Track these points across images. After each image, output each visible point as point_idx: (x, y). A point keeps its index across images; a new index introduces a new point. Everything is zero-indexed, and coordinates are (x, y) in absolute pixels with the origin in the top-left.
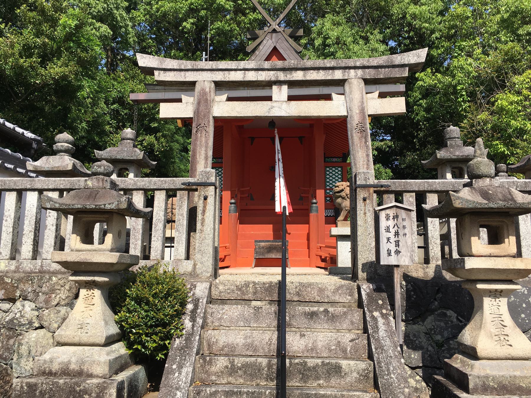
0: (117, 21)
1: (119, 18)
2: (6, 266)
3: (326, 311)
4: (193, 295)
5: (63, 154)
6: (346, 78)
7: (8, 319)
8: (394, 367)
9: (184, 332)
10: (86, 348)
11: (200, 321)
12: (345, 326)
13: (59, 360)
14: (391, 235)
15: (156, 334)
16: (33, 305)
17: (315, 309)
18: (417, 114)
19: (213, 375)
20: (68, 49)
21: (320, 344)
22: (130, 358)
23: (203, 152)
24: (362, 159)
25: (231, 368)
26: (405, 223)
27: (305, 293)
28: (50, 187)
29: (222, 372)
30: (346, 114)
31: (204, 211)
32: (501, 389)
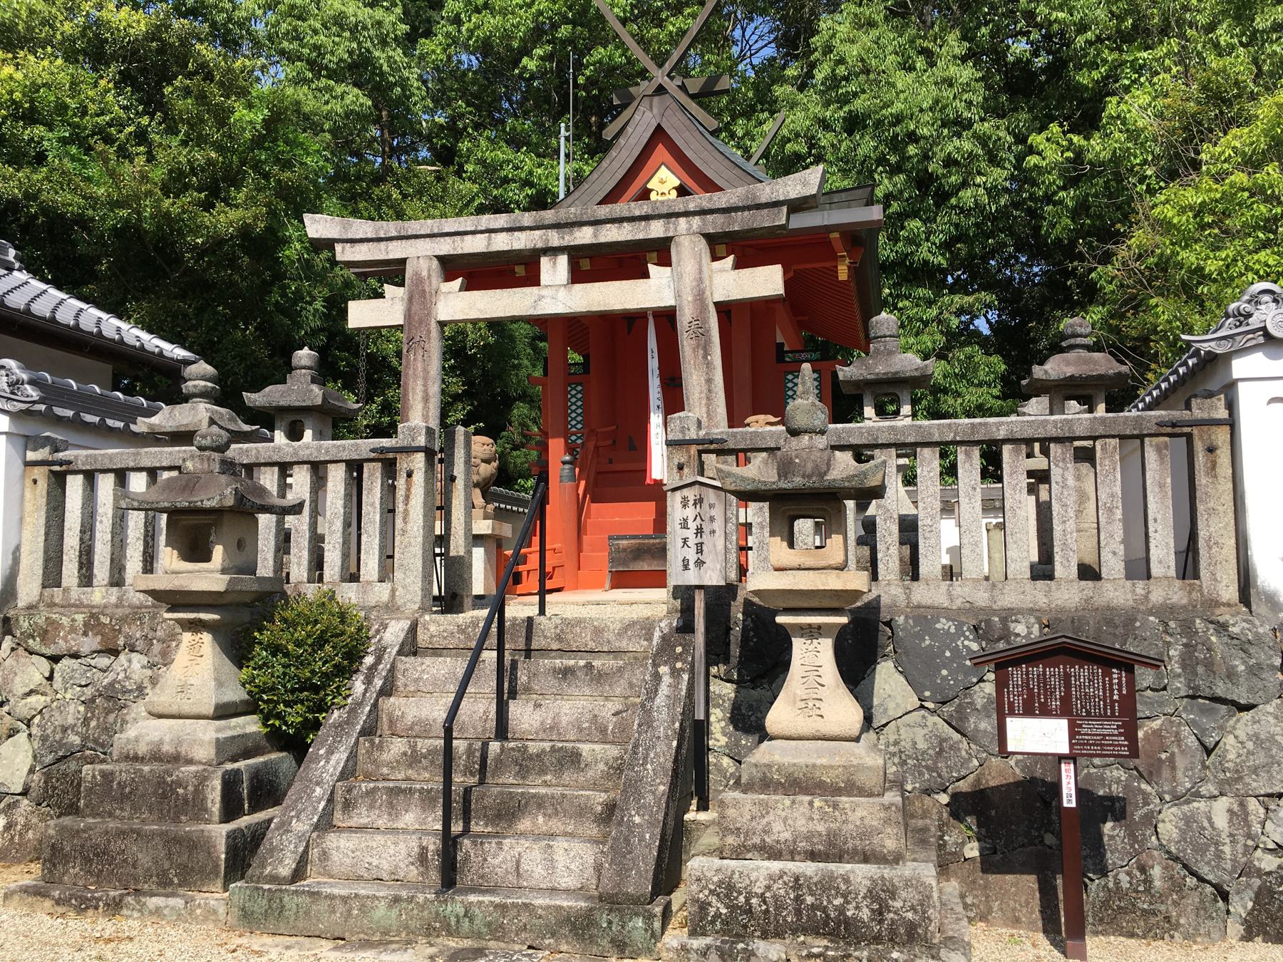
0: (382, 74)
1: (385, 68)
2: (104, 597)
3: (589, 666)
6: (671, 234)
7: (106, 682)
8: (656, 754)
9: (349, 700)
10: (188, 721)
11: (378, 683)
12: (618, 691)
13: (148, 739)
14: (690, 534)
15: (302, 702)
16: (144, 660)
17: (572, 662)
18: (1053, 226)
20: (257, 166)
21: (564, 720)
22: (268, 741)
23: (419, 389)
24: (698, 388)
25: (412, 756)
26: (713, 512)
27: (570, 636)
28: (164, 464)
29: (398, 762)
30: (671, 302)
31: (407, 497)
32: (790, 786)
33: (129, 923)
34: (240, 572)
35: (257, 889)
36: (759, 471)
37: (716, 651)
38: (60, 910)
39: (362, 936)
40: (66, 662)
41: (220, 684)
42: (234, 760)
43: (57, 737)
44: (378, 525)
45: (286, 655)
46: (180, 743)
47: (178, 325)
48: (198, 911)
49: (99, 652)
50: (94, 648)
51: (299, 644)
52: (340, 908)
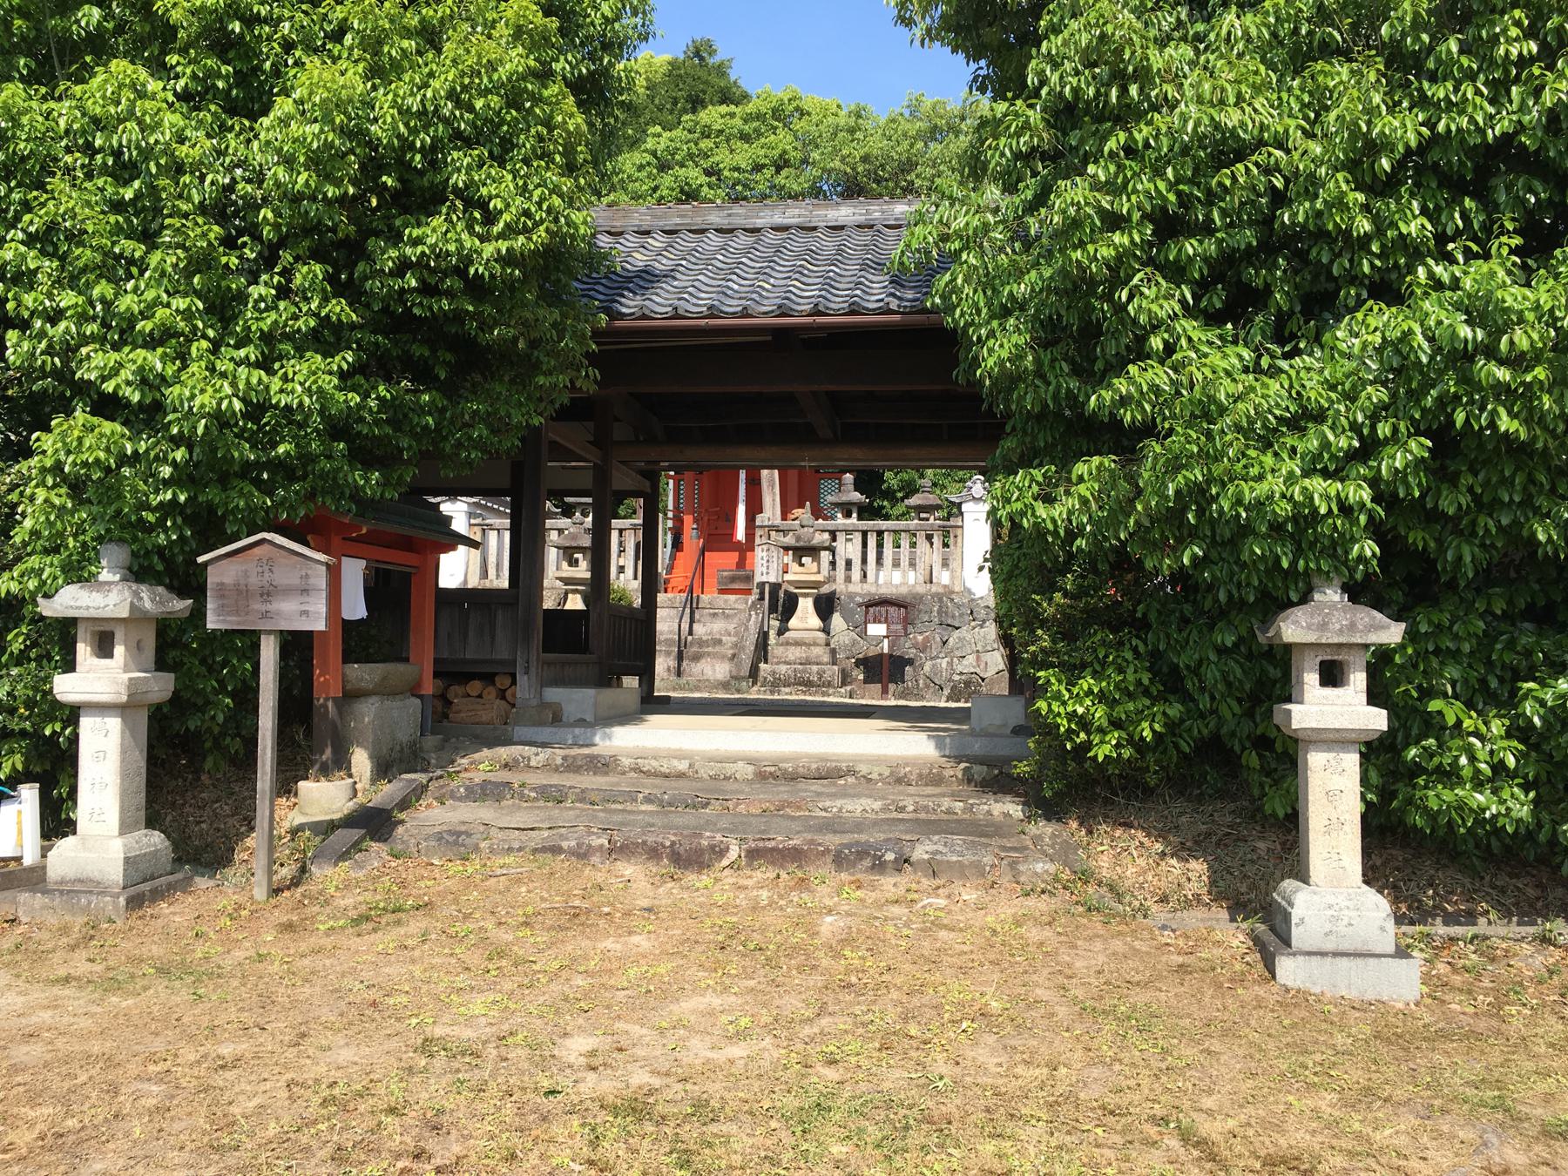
36: (789, 540)
37: (773, 608)
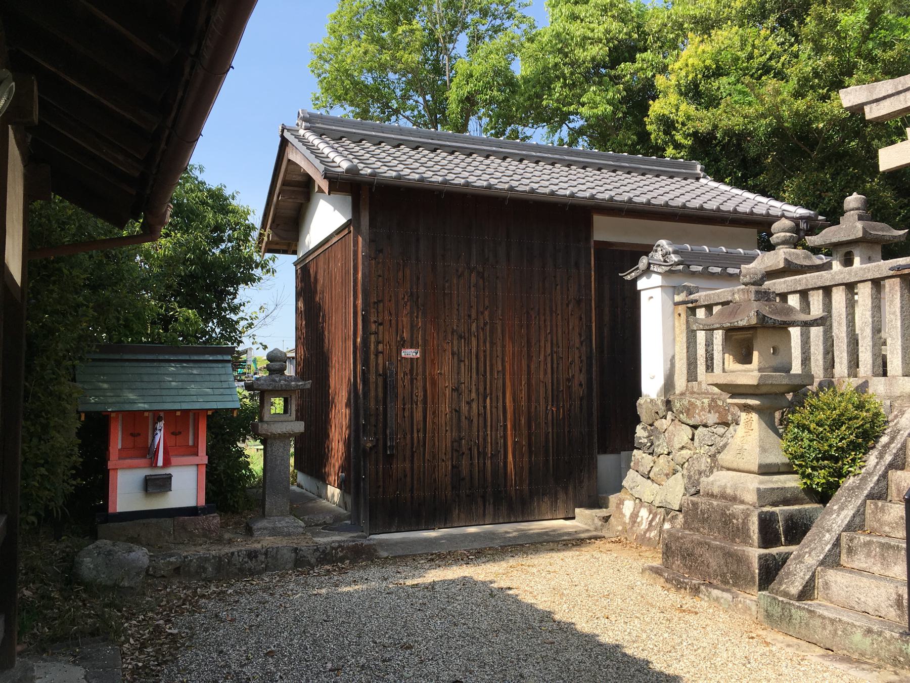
4: (898, 423)
5: (781, 246)
9: (863, 470)
11: (888, 458)
13: (718, 483)
19: (886, 525)
29: (896, 523)
33: (702, 603)
34: (776, 370)
35: (775, 599)
38: (668, 586)
39: (845, 652)
40: (700, 429)
41: (763, 450)
42: (774, 504)
43: (696, 477)
44: (899, 330)
45: (810, 432)
46: (736, 489)
47: (818, 190)
48: (740, 605)
49: (718, 424)
50: (715, 421)
51: (820, 424)
52: (830, 627)
